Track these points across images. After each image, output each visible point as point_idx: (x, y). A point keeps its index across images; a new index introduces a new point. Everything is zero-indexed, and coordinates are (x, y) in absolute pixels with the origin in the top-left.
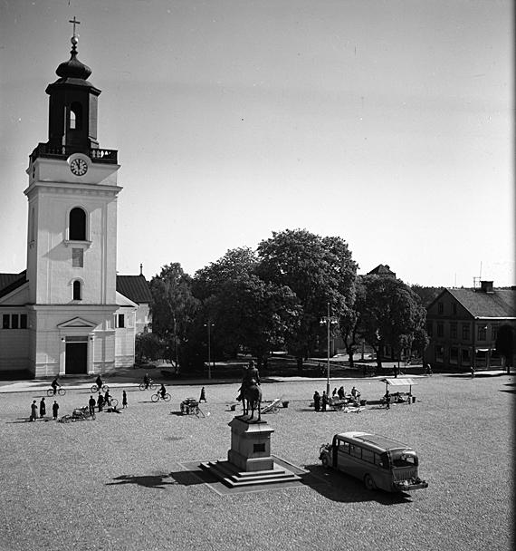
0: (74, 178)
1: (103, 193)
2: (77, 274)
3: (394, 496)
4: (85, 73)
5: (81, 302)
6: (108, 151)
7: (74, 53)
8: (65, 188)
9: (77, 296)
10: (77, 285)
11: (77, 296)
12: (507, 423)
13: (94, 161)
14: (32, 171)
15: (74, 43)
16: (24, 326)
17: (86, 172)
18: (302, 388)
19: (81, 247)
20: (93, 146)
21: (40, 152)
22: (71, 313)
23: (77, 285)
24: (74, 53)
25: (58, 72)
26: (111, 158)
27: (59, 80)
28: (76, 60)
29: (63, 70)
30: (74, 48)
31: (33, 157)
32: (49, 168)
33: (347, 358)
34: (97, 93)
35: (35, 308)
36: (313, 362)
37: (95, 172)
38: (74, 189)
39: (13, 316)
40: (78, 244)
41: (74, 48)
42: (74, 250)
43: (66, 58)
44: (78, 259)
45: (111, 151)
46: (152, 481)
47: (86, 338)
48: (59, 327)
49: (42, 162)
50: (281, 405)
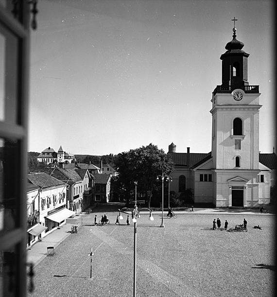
0: (236, 102)
2: (238, 153)
3: (263, 175)
4: (240, 46)
5: (240, 168)
6: (254, 86)
7: (234, 36)
9: (238, 164)
10: (238, 159)
11: (238, 164)
13: (246, 92)
14: (214, 100)
15: (234, 31)
16: (210, 180)
17: (242, 98)
20: (245, 84)
22: (234, 174)
23: (238, 159)
24: (234, 36)
25: (226, 48)
27: (227, 52)
28: (235, 40)
29: (229, 46)
30: (234, 34)
31: (214, 93)
32: (222, 98)
34: (247, 56)
35: (216, 171)
37: (247, 98)
39: (205, 175)
40: (238, 137)
41: (234, 34)
43: (230, 40)
44: (238, 145)
45: (255, 86)
47: (243, 187)
49: (219, 95)
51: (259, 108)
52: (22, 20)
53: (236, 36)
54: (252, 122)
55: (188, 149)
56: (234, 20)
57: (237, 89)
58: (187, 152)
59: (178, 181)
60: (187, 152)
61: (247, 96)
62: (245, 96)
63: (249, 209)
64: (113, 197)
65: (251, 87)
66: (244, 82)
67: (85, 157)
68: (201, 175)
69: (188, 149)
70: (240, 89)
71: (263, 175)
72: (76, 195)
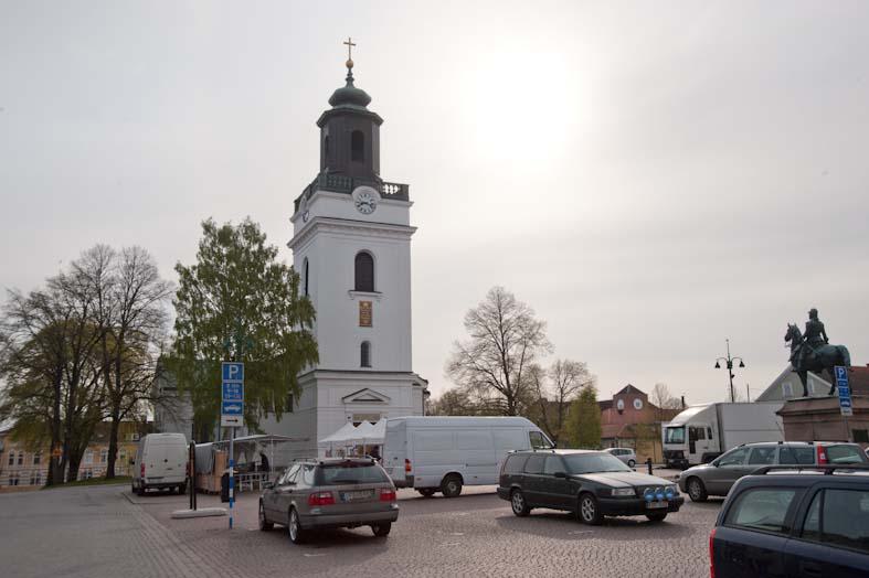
2: (366, 334)
3: (362, 324)
4: (363, 99)
5: (369, 369)
6: (398, 185)
7: (350, 79)
9: (365, 361)
10: (365, 347)
11: (365, 361)
12: (277, 554)
15: (350, 65)
18: (122, 457)
19: (369, 299)
22: (355, 383)
23: (365, 347)
24: (350, 79)
26: (402, 193)
29: (339, 98)
30: (350, 74)
32: (328, 204)
37: (385, 212)
40: (365, 297)
41: (350, 74)
42: (361, 304)
43: (343, 84)
44: (366, 319)
46: (350, 65)
48: (346, 401)
49: (323, 196)
50: (132, 466)
51: (412, 233)
56: (349, 44)
61: (386, 203)
62: (380, 203)
63: (152, 490)
64: (69, 481)
67: (599, 487)
68: (369, 324)
72: (291, 480)
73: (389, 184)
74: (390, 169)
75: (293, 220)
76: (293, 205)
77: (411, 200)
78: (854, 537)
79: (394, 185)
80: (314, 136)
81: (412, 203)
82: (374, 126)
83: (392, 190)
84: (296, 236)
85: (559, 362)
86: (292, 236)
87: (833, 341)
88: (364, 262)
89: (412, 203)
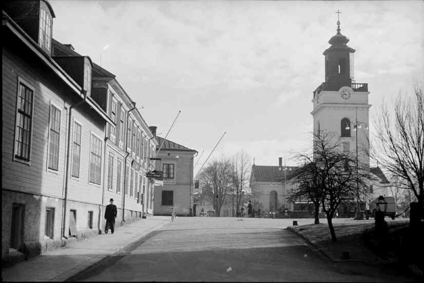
0: (343, 101)
1: (332, 109)
6: (362, 84)
7: (339, 30)
8: (334, 107)
13: (355, 90)
15: (339, 23)
20: (353, 82)
21: (325, 87)
24: (339, 30)
25: (330, 42)
26: (364, 88)
27: (331, 47)
28: (340, 34)
29: (332, 41)
30: (339, 27)
33: (312, 221)
34: (353, 51)
36: (109, 224)
38: (329, 107)
41: (339, 27)
43: (335, 33)
45: (364, 84)
46: (339, 23)
52: (38, 43)
53: (340, 30)
54: (111, 174)
55: (280, 159)
57: (343, 88)
58: (278, 165)
59: (269, 196)
60: (278, 165)
65: (356, 85)
66: (350, 79)
69: (280, 159)
70: (342, 86)
71: (53, 209)
73: (358, 84)
74: (358, 76)
75: (313, 101)
76: (313, 94)
77: (369, 91)
78: (92, 61)
79: (360, 84)
80: (322, 59)
81: (369, 92)
82: (350, 54)
83: (357, 87)
84: (314, 110)
85: (112, 232)
86: (313, 110)
87: (324, 56)
88: (345, 122)
89: (371, 106)
